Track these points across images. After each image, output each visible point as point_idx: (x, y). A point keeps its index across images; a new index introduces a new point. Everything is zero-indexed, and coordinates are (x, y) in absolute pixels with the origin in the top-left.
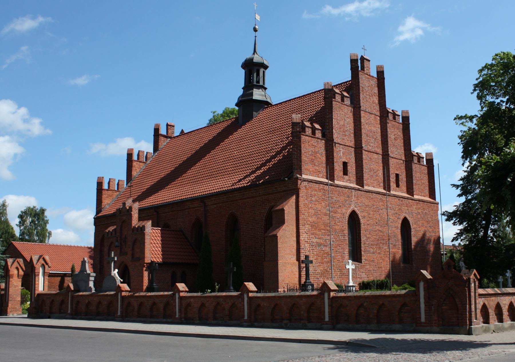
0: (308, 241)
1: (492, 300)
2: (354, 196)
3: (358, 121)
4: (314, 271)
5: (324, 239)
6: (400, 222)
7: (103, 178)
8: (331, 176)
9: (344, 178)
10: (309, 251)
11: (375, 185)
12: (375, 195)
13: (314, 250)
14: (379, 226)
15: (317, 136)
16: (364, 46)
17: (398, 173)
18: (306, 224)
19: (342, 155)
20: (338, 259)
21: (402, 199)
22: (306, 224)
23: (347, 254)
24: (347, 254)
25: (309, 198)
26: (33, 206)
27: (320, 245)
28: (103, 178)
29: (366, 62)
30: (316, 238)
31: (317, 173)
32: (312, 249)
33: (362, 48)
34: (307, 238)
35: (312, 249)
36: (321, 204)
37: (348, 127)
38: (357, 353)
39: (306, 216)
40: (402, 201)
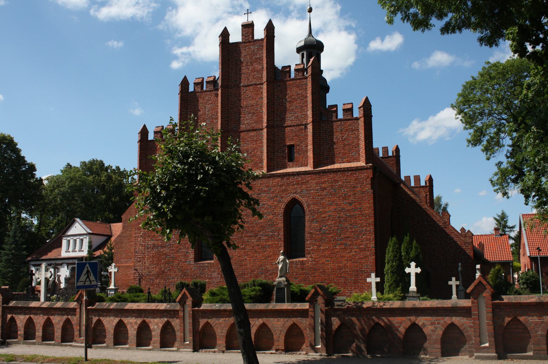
1: (410, 305)
23: (192, 253)
24: (192, 253)
32: (147, 252)
34: (143, 241)
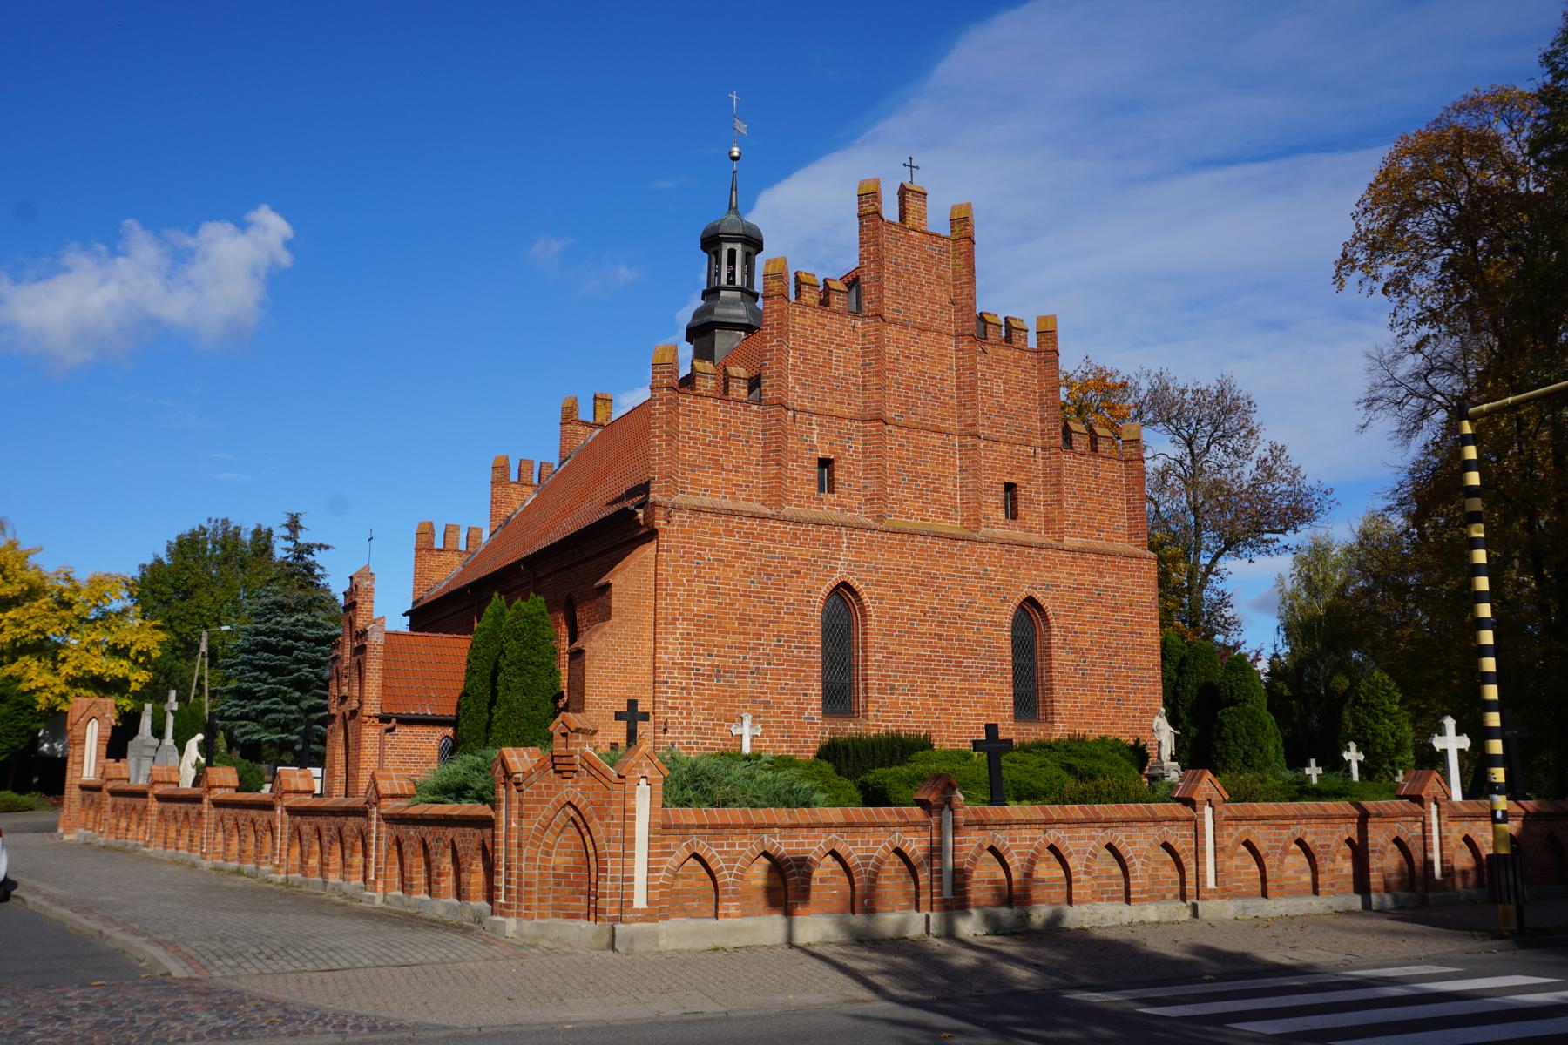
0: (682, 664)
2: (845, 545)
3: (871, 352)
4: (701, 738)
5: (739, 657)
6: (1010, 608)
7: (969, 205)
8: (776, 494)
9: (822, 500)
10: (683, 689)
11: (931, 516)
12: (920, 542)
13: (704, 685)
14: (933, 621)
15: (733, 394)
16: (911, 159)
17: (1013, 480)
18: (678, 619)
19: (815, 440)
20: (785, 708)
21: (1017, 549)
22: (678, 619)
23: (816, 695)
24: (816, 695)
25: (693, 553)
26: (1399, 483)
27: (718, 672)
28: (969, 205)
29: (913, 203)
30: (710, 655)
31: (729, 488)
32: (694, 684)
33: (905, 165)
34: (681, 654)
35: (694, 684)
36: (734, 566)
37: (841, 368)
38: (450, 816)
39: (679, 600)
40: (1019, 554)
